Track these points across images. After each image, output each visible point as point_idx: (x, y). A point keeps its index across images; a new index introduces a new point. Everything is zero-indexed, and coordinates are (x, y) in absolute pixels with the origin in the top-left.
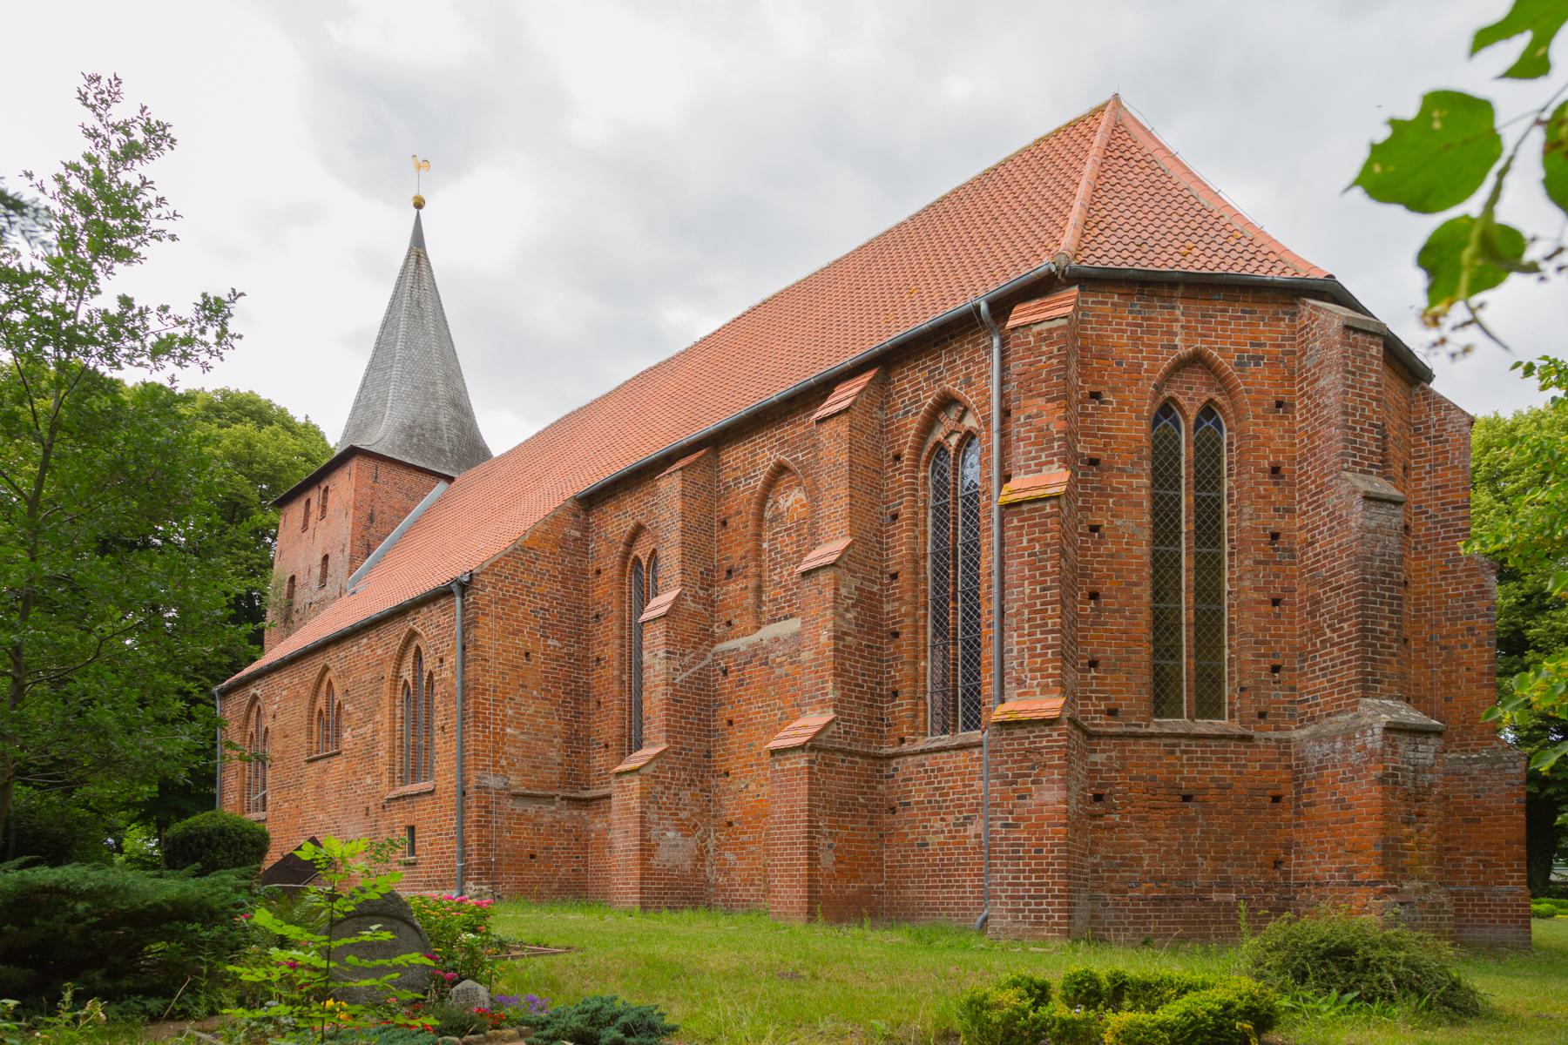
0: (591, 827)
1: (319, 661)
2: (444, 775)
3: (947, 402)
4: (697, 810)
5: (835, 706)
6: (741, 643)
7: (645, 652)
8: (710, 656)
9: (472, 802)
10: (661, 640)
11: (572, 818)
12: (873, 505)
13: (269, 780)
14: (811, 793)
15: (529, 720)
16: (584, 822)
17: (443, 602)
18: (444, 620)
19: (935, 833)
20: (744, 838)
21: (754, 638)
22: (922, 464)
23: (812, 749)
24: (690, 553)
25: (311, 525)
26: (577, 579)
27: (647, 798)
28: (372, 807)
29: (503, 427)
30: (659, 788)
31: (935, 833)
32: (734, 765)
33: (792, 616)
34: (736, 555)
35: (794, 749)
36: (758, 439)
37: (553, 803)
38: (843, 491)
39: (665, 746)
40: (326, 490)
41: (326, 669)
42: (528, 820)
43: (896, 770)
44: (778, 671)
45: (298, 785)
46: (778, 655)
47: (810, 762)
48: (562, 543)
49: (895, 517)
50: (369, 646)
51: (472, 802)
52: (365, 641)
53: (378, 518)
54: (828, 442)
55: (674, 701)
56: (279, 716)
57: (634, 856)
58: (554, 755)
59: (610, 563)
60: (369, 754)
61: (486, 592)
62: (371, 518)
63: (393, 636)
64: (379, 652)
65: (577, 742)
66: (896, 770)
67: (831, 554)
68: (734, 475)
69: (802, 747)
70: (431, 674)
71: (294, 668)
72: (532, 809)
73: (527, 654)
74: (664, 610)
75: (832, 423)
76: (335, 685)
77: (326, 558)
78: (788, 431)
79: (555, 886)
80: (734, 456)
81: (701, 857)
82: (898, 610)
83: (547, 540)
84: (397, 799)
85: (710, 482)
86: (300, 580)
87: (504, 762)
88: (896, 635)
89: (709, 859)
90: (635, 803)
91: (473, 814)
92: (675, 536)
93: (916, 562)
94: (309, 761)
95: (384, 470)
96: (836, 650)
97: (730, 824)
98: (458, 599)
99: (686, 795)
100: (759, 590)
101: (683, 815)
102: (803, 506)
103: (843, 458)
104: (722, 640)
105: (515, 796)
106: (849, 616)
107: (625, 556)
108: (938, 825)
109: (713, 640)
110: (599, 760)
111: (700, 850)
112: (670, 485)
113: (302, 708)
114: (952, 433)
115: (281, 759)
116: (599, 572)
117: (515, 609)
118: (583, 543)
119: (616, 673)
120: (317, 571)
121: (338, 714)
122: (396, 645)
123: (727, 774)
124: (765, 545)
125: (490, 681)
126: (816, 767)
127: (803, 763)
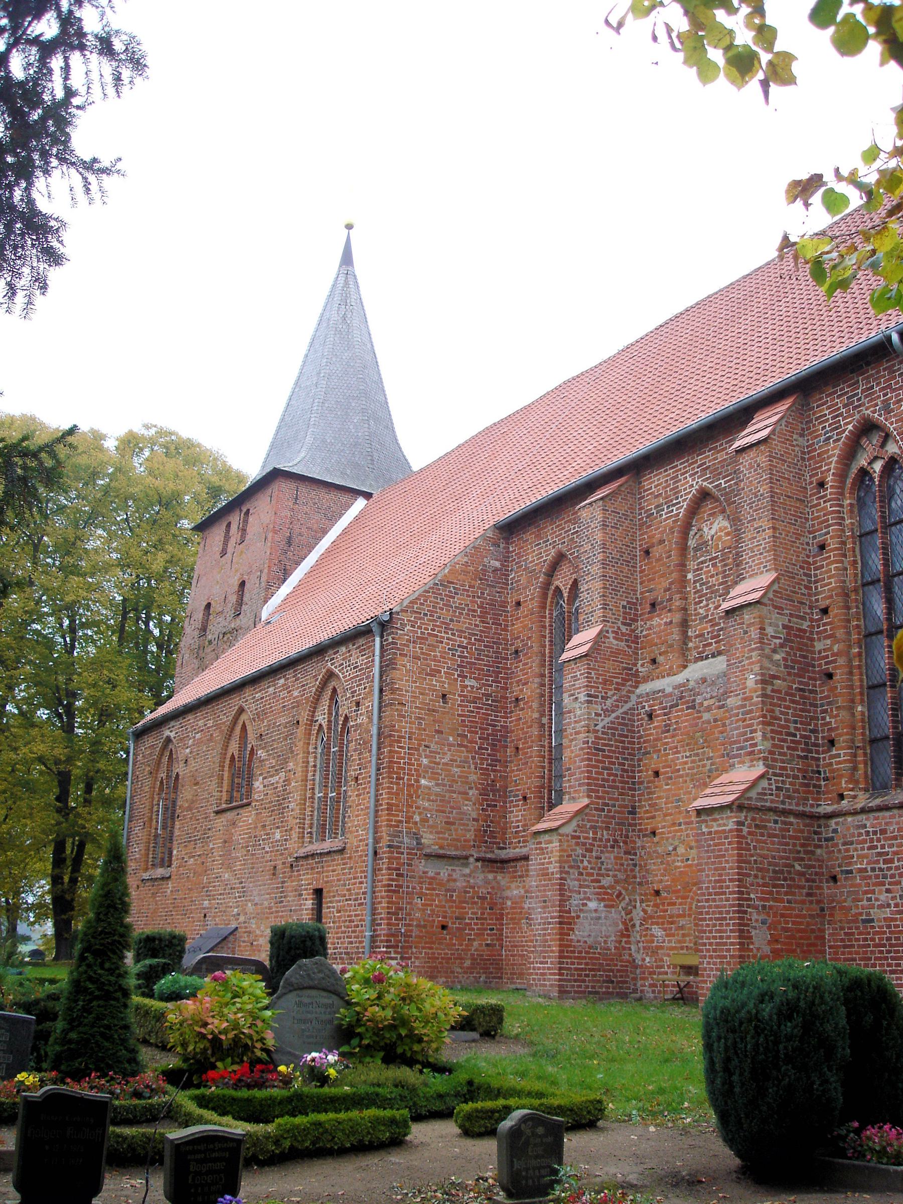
0: (508, 893)
1: (235, 702)
2: (359, 830)
3: (868, 428)
4: (621, 876)
5: (765, 759)
6: (666, 684)
7: (565, 695)
8: (633, 698)
9: (384, 864)
10: (582, 681)
11: (487, 882)
12: (798, 536)
13: (177, 833)
14: (741, 860)
15: (443, 773)
16: (501, 889)
17: (361, 641)
18: (361, 661)
19: (881, 907)
20: (671, 910)
21: (680, 678)
22: (847, 491)
23: (741, 808)
24: (611, 587)
25: (230, 550)
26: (494, 613)
27: (567, 862)
28: (279, 867)
29: (426, 432)
30: (579, 851)
31: (881, 907)
32: (661, 825)
33: (720, 653)
34: (660, 587)
35: (722, 808)
36: (679, 464)
37: (466, 865)
38: (765, 524)
39: (586, 801)
40: (247, 513)
41: (241, 710)
42: (441, 884)
43: (835, 831)
44: (706, 716)
45: (205, 840)
46: (705, 699)
47: (740, 823)
48: (481, 575)
49: (822, 547)
50: (285, 687)
51: (384, 864)
52: (282, 681)
53: (296, 540)
54: (749, 468)
55: (595, 750)
56: (191, 761)
57: (552, 929)
58: (470, 809)
59: (531, 594)
60: (279, 806)
61: (405, 631)
62: (289, 542)
63: (309, 678)
64: (296, 693)
65: (494, 795)
66: (835, 831)
67: (755, 590)
68: (656, 502)
69: (729, 807)
70: (346, 719)
71: (208, 709)
72: (444, 871)
73: (444, 696)
74: (585, 649)
75: (752, 453)
76: (249, 728)
77: (243, 584)
78: (708, 457)
79: (468, 963)
80: (656, 482)
81: (626, 932)
82: (830, 649)
83: (466, 573)
84: (306, 857)
85: (632, 508)
86: (216, 607)
87: (417, 818)
88: (830, 676)
89: (636, 936)
90: (553, 868)
91: (384, 877)
92: (596, 569)
93: (847, 595)
94: (217, 813)
95: (304, 490)
96: (764, 695)
97: (657, 893)
98: (378, 639)
99: (609, 858)
100: (684, 624)
101: (606, 881)
102: (727, 534)
103: (764, 489)
104: (646, 679)
105: (428, 856)
106: (777, 657)
107: (547, 585)
108: (884, 897)
109: (637, 679)
110: (517, 815)
111: (624, 923)
112: (590, 512)
113: (213, 755)
114: (876, 458)
115: (190, 809)
116: (518, 604)
117: (433, 647)
118: (503, 573)
119: (536, 715)
120: (233, 599)
121: (250, 760)
122: (313, 686)
123: (654, 833)
124: (690, 576)
125: (405, 727)
126: (745, 830)
127: (731, 826)
